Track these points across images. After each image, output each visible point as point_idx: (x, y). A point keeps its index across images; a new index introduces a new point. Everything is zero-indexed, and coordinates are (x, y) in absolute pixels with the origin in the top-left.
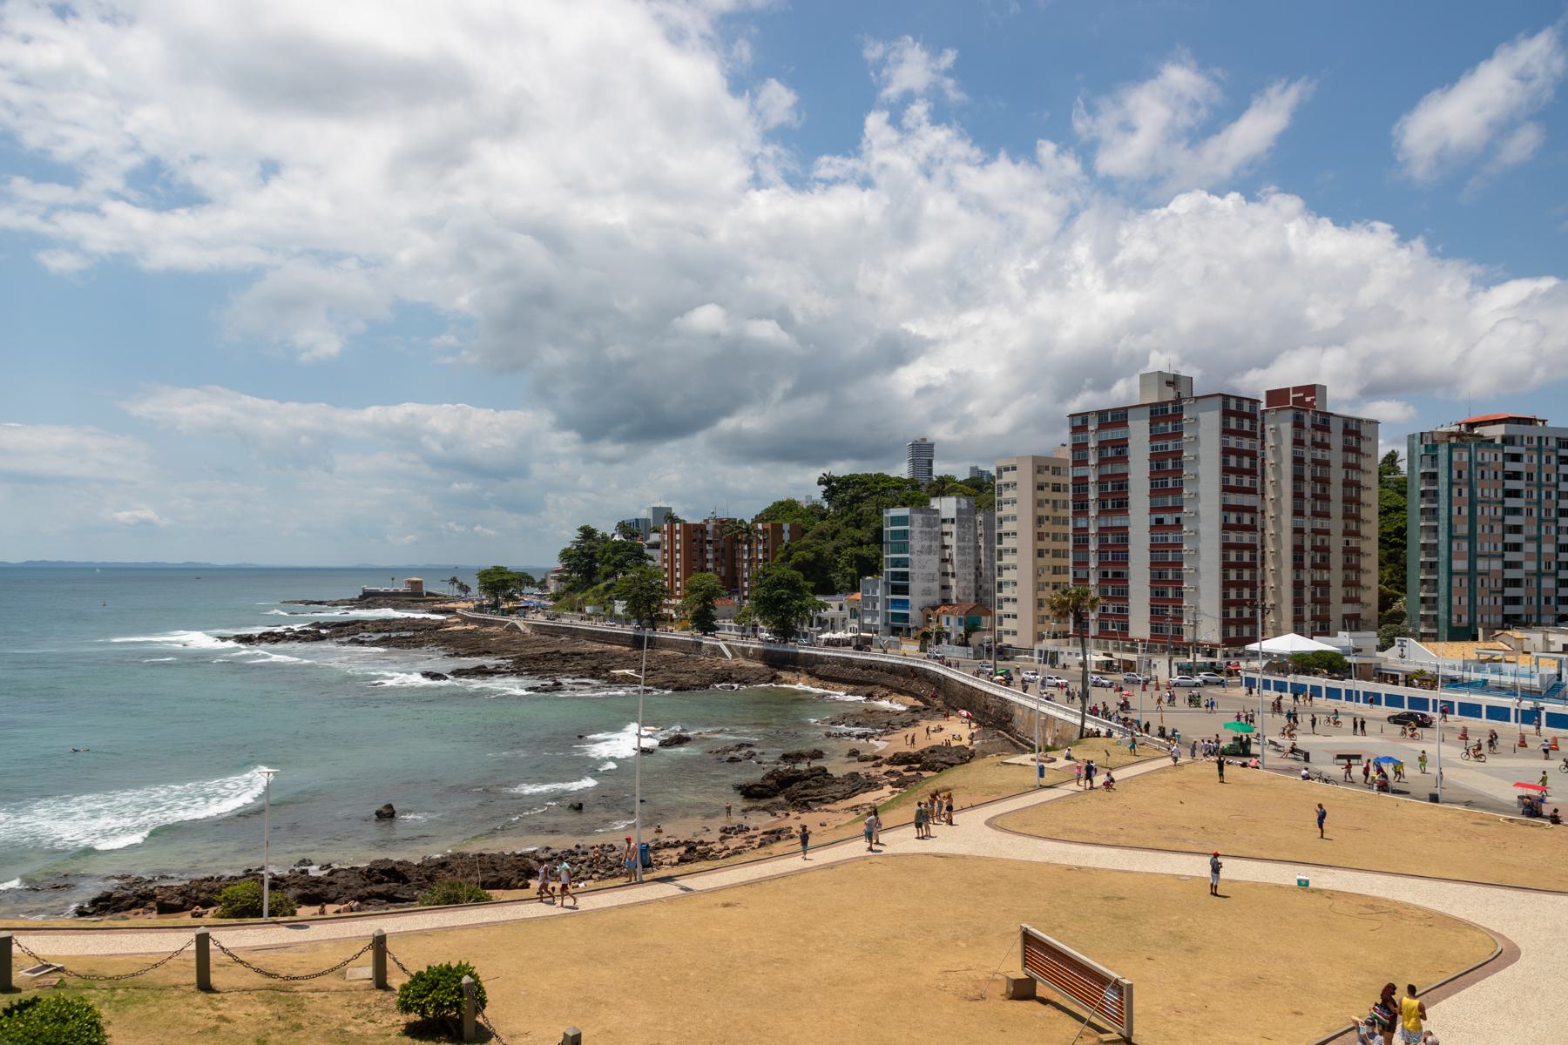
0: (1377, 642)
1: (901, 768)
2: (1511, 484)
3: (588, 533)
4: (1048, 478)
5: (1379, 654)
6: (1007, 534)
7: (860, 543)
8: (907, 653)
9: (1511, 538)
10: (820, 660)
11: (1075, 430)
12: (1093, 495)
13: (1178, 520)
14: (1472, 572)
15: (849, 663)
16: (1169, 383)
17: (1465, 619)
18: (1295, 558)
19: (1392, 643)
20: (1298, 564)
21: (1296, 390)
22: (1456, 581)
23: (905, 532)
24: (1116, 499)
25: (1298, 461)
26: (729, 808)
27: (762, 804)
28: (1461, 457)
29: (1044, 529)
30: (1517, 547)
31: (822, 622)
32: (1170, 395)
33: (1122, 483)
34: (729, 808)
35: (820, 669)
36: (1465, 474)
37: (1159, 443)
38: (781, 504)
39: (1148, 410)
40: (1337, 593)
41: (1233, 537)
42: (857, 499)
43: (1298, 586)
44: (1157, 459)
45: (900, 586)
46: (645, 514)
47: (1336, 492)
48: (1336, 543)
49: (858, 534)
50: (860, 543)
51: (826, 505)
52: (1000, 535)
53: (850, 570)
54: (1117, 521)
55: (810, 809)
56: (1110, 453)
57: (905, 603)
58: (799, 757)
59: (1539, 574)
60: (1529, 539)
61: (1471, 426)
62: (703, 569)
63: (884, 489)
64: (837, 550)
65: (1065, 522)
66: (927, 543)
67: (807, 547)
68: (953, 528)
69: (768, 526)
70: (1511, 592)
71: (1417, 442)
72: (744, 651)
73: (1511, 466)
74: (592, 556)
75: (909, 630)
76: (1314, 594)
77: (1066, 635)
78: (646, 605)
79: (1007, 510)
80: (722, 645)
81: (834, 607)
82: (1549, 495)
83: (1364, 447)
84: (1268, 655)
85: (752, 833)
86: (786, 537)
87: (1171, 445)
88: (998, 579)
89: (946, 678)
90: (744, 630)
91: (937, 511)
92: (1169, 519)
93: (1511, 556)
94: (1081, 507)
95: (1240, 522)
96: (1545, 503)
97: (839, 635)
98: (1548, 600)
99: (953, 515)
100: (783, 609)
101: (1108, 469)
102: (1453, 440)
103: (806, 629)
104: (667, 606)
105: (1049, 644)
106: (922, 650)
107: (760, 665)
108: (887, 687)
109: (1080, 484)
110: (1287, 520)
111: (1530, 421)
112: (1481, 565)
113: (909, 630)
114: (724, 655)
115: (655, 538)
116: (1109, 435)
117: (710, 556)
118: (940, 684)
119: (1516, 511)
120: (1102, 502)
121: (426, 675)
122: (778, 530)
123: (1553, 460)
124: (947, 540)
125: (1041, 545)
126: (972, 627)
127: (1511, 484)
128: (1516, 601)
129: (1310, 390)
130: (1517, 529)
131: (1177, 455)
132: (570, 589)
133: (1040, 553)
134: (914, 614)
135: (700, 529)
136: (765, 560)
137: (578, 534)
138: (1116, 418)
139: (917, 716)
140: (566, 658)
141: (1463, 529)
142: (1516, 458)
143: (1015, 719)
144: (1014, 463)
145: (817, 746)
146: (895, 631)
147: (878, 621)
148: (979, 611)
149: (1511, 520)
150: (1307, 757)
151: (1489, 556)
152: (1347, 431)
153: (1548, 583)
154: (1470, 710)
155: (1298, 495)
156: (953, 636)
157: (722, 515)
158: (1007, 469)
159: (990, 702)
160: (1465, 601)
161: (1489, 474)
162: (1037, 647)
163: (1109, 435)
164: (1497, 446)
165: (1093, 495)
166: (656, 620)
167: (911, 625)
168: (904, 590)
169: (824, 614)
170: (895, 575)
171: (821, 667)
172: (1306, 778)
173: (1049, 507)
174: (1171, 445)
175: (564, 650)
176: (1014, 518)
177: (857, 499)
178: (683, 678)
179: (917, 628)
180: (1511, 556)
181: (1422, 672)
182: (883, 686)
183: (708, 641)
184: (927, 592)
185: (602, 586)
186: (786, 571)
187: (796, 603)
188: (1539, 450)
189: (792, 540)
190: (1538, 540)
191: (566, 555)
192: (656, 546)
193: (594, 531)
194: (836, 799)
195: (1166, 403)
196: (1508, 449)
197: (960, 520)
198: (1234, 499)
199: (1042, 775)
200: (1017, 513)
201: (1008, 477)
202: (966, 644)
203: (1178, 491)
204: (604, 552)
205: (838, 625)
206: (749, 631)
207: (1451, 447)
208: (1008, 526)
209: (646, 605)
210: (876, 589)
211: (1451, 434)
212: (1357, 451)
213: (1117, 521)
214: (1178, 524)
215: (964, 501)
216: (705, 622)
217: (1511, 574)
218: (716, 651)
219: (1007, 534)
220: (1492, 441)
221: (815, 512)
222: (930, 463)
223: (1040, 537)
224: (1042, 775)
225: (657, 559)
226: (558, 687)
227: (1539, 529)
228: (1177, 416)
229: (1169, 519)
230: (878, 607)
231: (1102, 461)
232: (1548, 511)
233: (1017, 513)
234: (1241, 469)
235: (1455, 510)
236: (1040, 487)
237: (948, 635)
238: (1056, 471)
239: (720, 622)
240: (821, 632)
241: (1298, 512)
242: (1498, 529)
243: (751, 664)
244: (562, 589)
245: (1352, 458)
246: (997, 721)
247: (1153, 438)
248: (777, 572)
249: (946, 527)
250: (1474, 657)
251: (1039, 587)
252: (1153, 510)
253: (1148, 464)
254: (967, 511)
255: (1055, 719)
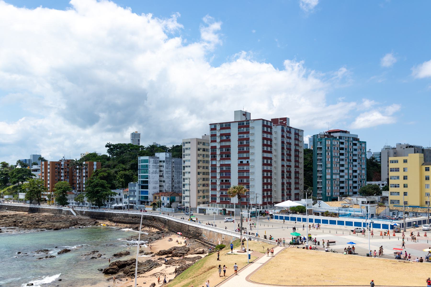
1: (164, 257)
2: (342, 152)
4: (201, 146)
5: (313, 206)
6: (187, 167)
8: (149, 211)
9: (342, 168)
10: (114, 215)
11: (212, 129)
12: (218, 152)
13: (248, 162)
14: (332, 179)
15: (127, 216)
16: (244, 115)
17: (330, 194)
20: (283, 178)
21: (281, 119)
23: (147, 166)
25: (283, 142)
29: (200, 165)
30: (343, 171)
31: (112, 200)
32: (244, 119)
33: (228, 148)
35: (115, 219)
37: (241, 135)
38: (91, 154)
39: (237, 123)
40: (293, 186)
41: (265, 168)
42: (122, 152)
43: (283, 184)
44: (241, 140)
45: (145, 185)
47: (293, 153)
48: (293, 170)
49: (124, 166)
50: (125, 170)
52: (184, 167)
54: (227, 162)
56: (224, 138)
58: (120, 255)
59: (348, 180)
60: (346, 169)
61: (330, 133)
62: (60, 180)
64: (116, 172)
66: (155, 170)
67: (105, 171)
68: (164, 164)
69: (88, 162)
70: (342, 185)
71: (316, 137)
72: (81, 213)
73: (342, 146)
74: (7, 174)
75: (148, 202)
79: (187, 158)
80: (71, 210)
81: (120, 193)
82: (351, 155)
84: (279, 208)
87: (245, 136)
88: (183, 183)
89: (169, 220)
91: (158, 158)
92: (245, 162)
93: (342, 174)
94: (214, 157)
95: (267, 162)
96: (350, 158)
97: (120, 205)
98: (351, 187)
99: (164, 159)
100: (99, 194)
101: (224, 144)
102: (326, 137)
104: (43, 195)
105: (202, 206)
106: (154, 210)
109: (214, 148)
110: (280, 163)
111: (346, 132)
112: (334, 177)
113: (148, 202)
114: (72, 214)
115: (35, 167)
116: (224, 132)
119: (342, 160)
120: (221, 154)
123: (352, 145)
126: (172, 201)
127: (342, 152)
128: (342, 188)
129: (285, 119)
130: (343, 165)
131: (248, 139)
133: (199, 173)
134: (151, 197)
135: (59, 163)
136: (86, 176)
138: (226, 126)
141: (329, 166)
142: (342, 143)
143: (203, 235)
144: (189, 141)
145: (128, 249)
146: (142, 203)
149: (342, 163)
151: (336, 174)
152: (296, 134)
153: (351, 182)
155: (283, 154)
156: (165, 204)
157: (67, 158)
158: (187, 143)
159: (190, 228)
160: (330, 188)
161: (336, 148)
162: (198, 207)
163: (224, 132)
164: (338, 140)
165: (218, 152)
166: (40, 201)
168: (147, 187)
170: (143, 182)
171: (115, 218)
172: (327, 251)
173: (201, 157)
174: (245, 136)
176: (189, 161)
177: (122, 152)
178: (57, 224)
179: (151, 202)
180: (342, 174)
181: (327, 212)
184: (155, 188)
186: (96, 180)
188: (348, 141)
189: (97, 168)
190: (348, 169)
192: (36, 170)
195: (244, 121)
196: (341, 141)
197: (166, 161)
199: (249, 258)
200: (190, 159)
201: (187, 146)
202: (170, 207)
203: (248, 152)
205: (123, 200)
207: (326, 139)
209: (35, 195)
210: (136, 187)
212: (298, 140)
213: (227, 162)
214: (248, 164)
215: (168, 154)
216: (63, 201)
217: (342, 179)
218: (69, 212)
219: (187, 167)
220: (336, 138)
221: (104, 157)
222: (139, 140)
224: (249, 258)
227: (348, 166)
228: (248, 126)
229: (245, 162)
230: (136, 194)
231: (222, 141)
232: (350, 160)
234: (267, 144)
235: (327, 159)
237: (163, 204)
241: (283, 160)
242: (338, 166)
243: (85, 218)
245: (297, 143)
246: (195, 235)
247: (239, 133)
248: (97, 181)
250: (341, 206)
252: (239, 158)
254: (169, 158)
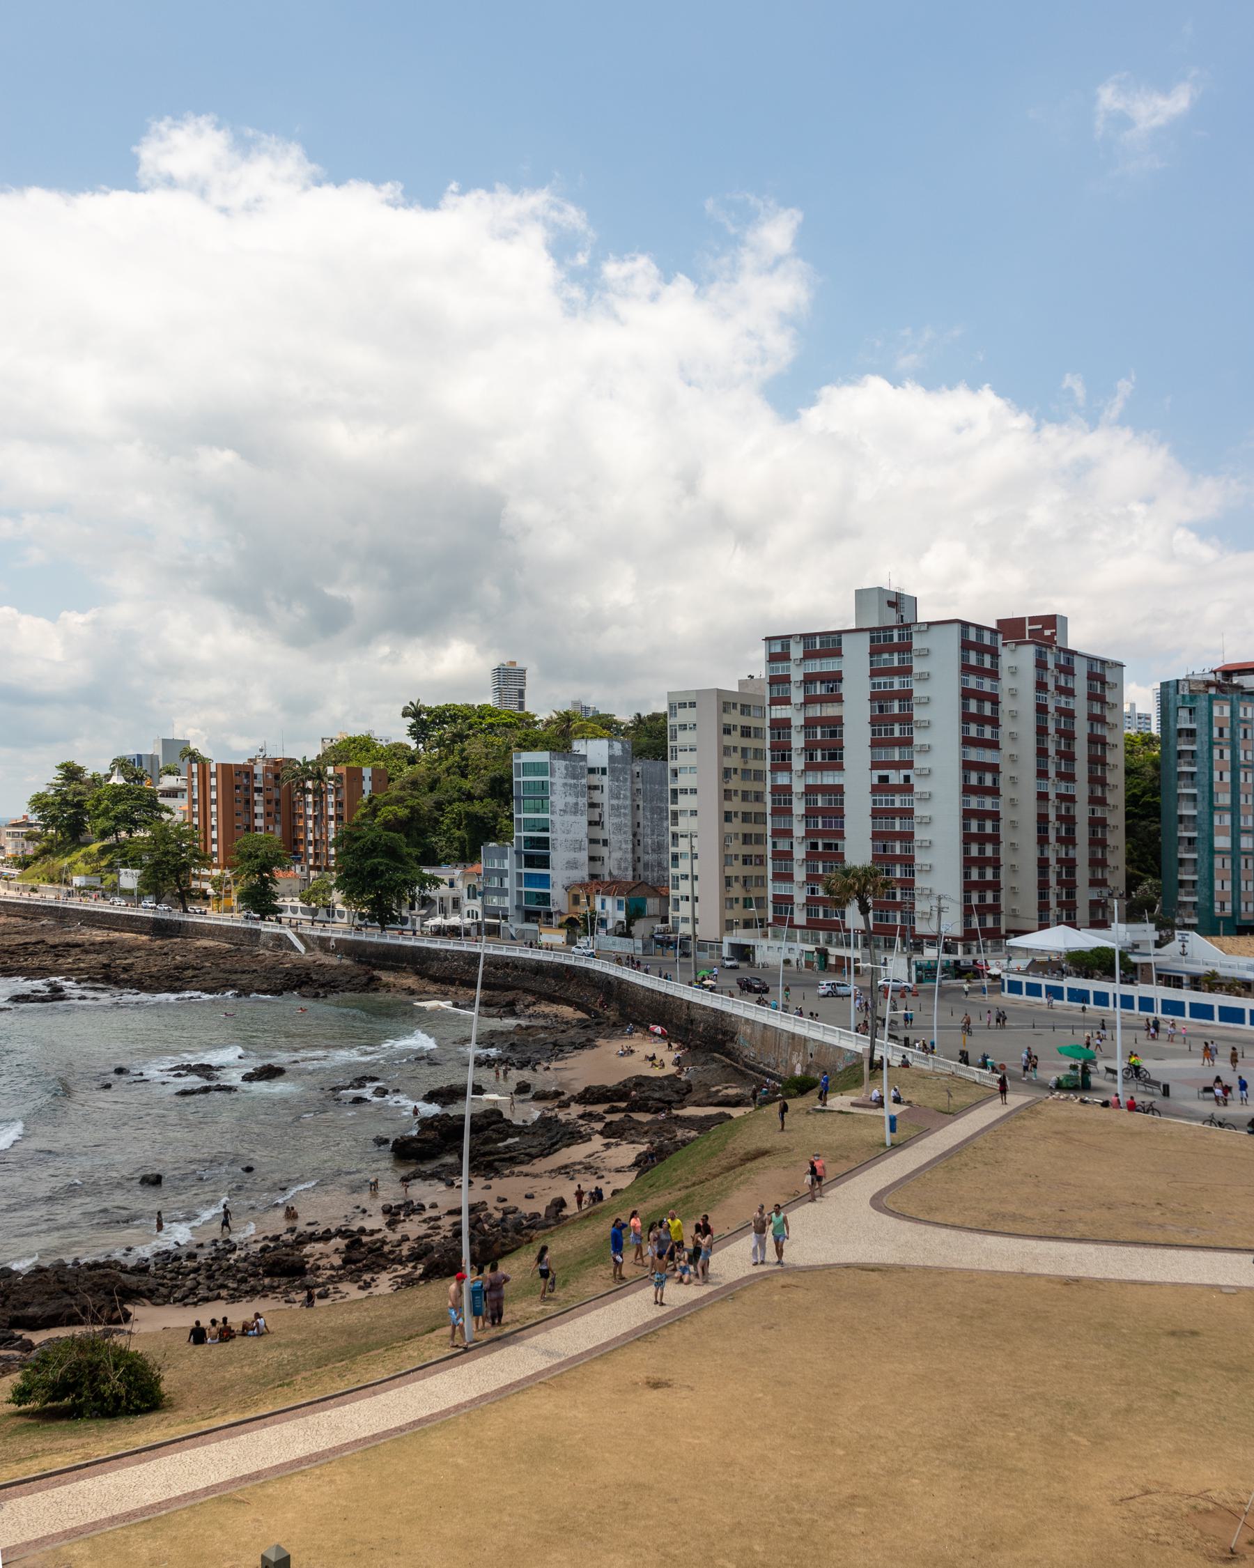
0: (1156, 936)
1: (599, 1109)
3: (71, 773)
4: (735, 718)
6: (684, 791)
7: (470, 797)
11: (773, 658)
13: (907, 778)
16: (891, 604)
17: (1228, 906)
18: (1039, 830)
19: (1170, 939)
21: (1033, 620)
22: (1218, 862)
24: (828, 751)
25: (1041, 709)
26: (375, 1184)
27: (428, 1167)
28: (1222, 712)
31: (426, 902)
32: (891, 618)
34: (375, 1184)
35: (435, 968)
36: (1227, 732)
37: (882, 680)
40: (1082, 874)
41: (974, 803)
42: (460, 737)
43: (1043, 864)
45: (537, 855)
46: (151, 748)
47: (1081, 749)
48: (1082, 812)
49: (467, 785)
51: (412, 744)
52: (674, 792)
53: (458, 833)
54: (829, 779)
55: (498, 1173)
56: (820, 689)
57: (544, 881)
61: (1228, 673)
63: (491, 726)
64: (439, 806)
65: (759, 776)
67: (400, 801)
68: (605, 781)
69: (342, 769)
71: (1172, 691)
72: (323, 943)
74: (79, 805)
75: (549, 915)
76: (1059, 874)
77: (762, 922)
78: (170, 872)
83: (1110, 697)
85: (430, 1213)
86: (367, 786)
87: (897, 683)
89: (621, 982)
90: (314, 912)
91: (584, 758)
92: (896, 778)
95: (980, 780)
97: (454, 920)
99: (604, 763)
101: (816, 711)
102: (1212, 691)
103: (405, 913)
104: (196, 877)
105: (741, 937)
107: (346, 962)
108: (533, 993)
113: (549, 915)
114: (294, 948)
115: (168, 782)
116: (817, 666)
117: (259, 809)
118: (611, 989)
120: (809, 749)
121: (431, 1097)
122: (355, 775)
124: (597, 797)
125: (728, 806)
129: (1050, 621)
132: (45, 852)
133: (728, 817)
134: (559, 898)
135: (246, 772)
137: (58, 773)
138: (825, 645)
139: (590, 1033)
140: (60, 950)
143: (740, 1039)
146: (529, 916)
147: (508, 903)
148: (644, 892)
150: (1166, 1091)
152: (1092, 676)
154: (1202, 1011)
156: (610, 926)
157: (278, 754)
158: (683, 705)
159: (697, 1015)
163: (817, 666)
166: (185, 897)
167: (553, 909)
168: (544, 862)
169: (433, 893)
171: (436, 964)
175: (51, 940)
177: (460, 737)
182: (527, 991)
183: (268, 927)
184: (573, 865)
185: (94, 848)
187: (400, 876)
191: (39, 803)
192: (173, 793)
193: (80, 770)
194: (532, 1157)
195: (891, 628)
197: (613, 770)
198: (975, 755)
200: (696, 766)
201: (684, 716)
202: (627, 934)
204: (99, 801)
206: (322, 915)
208: (683, 781)
209: (170, 872)
210: (505, 860)
211: (1209, 684)
212: (1101, 699)
213: (829, 779)
216: (261, 901)
218: (280, 940)
219: (684, 791)
223: (727, 795)
225: (178, 811)
226: (57, 994)
229: (896, 778)
233: (696, 766)
234: (980, 714)
236: (727, 731)
237: (603, 922)
238: (745, 709)
239: (279, 902)
240: (426, 917)
243: (333, 960)
244: (31, 849)
245: (1097, 710)
247: (874, 673)
249: (596, 779)
251: (726, 860)
252: (875, 765)
253: (867, 706)
255: (805, 1040)
